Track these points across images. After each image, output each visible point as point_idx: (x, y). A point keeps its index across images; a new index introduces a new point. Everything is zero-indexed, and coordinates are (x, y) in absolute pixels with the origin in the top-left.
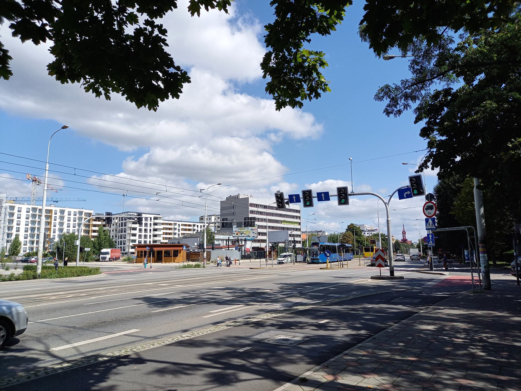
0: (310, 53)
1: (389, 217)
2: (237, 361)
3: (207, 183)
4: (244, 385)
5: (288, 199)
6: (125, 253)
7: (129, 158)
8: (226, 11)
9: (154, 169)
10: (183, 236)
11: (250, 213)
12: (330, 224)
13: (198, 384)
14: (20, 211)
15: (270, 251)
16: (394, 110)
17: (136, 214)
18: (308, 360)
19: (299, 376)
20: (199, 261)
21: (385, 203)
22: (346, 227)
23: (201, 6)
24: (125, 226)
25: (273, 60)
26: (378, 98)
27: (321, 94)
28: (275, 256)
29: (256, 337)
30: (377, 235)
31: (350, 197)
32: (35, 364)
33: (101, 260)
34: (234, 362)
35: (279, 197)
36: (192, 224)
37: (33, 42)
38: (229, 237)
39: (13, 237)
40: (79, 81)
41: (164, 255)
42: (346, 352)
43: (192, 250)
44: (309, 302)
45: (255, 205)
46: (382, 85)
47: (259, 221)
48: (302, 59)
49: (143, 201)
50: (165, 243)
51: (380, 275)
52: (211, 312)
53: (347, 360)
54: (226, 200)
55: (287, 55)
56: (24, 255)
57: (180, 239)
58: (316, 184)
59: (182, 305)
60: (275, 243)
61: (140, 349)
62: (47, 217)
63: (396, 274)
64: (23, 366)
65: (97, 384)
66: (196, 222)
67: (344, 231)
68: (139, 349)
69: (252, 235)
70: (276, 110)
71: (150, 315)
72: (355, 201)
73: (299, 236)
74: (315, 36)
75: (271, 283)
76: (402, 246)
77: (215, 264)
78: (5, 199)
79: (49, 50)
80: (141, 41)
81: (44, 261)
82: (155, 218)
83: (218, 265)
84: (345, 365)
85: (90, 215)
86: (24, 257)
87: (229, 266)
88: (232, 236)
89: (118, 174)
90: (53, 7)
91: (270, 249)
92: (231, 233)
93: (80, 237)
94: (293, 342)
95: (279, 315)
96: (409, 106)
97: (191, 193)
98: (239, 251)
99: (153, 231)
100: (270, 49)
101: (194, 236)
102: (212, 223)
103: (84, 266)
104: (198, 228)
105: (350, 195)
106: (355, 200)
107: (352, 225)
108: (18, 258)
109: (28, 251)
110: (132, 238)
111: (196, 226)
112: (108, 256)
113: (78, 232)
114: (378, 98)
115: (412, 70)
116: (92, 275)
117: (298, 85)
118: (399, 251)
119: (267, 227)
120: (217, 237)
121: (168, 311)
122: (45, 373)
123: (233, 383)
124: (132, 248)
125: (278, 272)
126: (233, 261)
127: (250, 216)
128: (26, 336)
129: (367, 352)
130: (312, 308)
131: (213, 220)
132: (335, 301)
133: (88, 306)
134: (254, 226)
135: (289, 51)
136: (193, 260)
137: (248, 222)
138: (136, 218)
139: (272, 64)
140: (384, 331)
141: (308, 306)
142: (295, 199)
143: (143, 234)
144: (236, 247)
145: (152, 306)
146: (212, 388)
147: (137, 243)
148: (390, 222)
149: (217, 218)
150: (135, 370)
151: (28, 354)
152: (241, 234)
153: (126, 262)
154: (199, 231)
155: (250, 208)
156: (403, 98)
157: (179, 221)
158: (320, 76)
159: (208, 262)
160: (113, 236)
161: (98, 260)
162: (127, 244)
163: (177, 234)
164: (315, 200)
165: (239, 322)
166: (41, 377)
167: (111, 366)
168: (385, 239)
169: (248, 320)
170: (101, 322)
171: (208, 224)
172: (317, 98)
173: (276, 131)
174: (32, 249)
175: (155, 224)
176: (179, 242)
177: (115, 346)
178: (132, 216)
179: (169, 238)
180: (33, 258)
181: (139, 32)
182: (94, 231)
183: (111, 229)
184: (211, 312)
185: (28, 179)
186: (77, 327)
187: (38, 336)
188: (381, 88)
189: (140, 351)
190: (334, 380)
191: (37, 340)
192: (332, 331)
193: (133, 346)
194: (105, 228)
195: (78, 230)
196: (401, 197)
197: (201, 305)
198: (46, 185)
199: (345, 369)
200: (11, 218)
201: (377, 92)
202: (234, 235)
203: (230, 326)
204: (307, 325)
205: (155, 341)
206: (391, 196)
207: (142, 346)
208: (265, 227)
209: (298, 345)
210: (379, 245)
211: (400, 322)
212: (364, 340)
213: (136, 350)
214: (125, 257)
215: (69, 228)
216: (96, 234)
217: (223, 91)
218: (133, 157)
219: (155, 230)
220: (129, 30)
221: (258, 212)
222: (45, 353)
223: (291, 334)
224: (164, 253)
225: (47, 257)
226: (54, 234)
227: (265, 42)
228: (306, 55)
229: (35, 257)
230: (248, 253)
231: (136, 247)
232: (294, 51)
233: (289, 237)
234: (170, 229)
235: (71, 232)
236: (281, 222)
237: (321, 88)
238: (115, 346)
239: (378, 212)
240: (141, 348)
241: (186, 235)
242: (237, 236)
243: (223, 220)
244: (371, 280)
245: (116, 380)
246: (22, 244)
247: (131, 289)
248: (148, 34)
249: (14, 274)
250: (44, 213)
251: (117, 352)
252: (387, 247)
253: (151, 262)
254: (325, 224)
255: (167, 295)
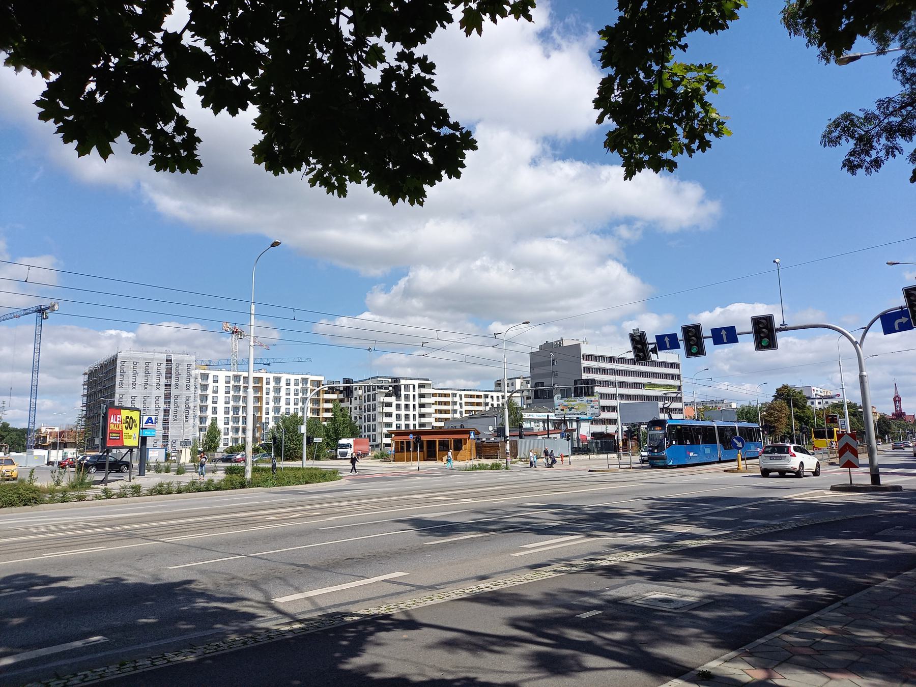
0: (688, 69)
1: (864, 370)
2: (575, 634)
3: (505, 321)
4: (593, 678)
5: (655, 343)
6: (376, 445)
7: (376, 287)
8: (529, 18)
9: (416, 303)
10: (468, 415)
11: (584, 372)
12: (741, 387)
13: (512, 670)
14: (217, 382)
15: (625, 439)
16: (864, 161)
17: (390, 380)
18: (711, 640)
19: (697, 667)
20: (497, 458)
21: (855, 343)
22: (774, 393)
23: (483, 16)
24: (374, 400)
25: (618, 91)
26: (830, 140)
27: (711, 142)
28: (635, 449)
29: (608, 593)
30: (841, 406)
31: (778, 334)
32: (252, 623)
33: (340, 457)
34: (572, 635)
35: (638, 341)
36: (482, 393)
37: (228, 112)
38: (548, 415)
39: (209, 422)
40: (299, 169)
41: (439, 449)
42: (788, 628)
43: (484, 439)
44: (706, 533)
45: (593, 357)
46: (836, 115)
47: (602, 385)
48: (673, 82)
49: (401, 358)
50: (440, 427)
51: (849, 483)
52: (524, 546)
53: (792, 644)
54: (539, 350)
55: (644, 78)
56: (225, 451)
57: (463, 419)
58: (710, 312)
59: (475, 532)
60: (634, 425)
61: (411, 605)
62: (258, 389)
63: (885, 481)
64: (234, 624)
65: (346, 659)
66: (489, 391)
67: (770, 399)
68: (408, 605)
69: (589, 411)
70: (625, 179)
71: (423, 550)
72: (791, 341)
73: (680, 411)
74: (696, 38)
75: (631, 497)
76: (893, 426)
77: (525, 463)
78: (194, 364)
79: (253, 124)
80: (393, 89)
81: (255, 460)
82: (421, 386)
83: (531, 465)
84: (787, 653)
85: (318, 383)
86: (225, 453)
87: (550, 467)
88: (554, 414)
89: (359, 314)
90: (256, 51)
91: (625, 435)
92: (552, 408)
93: (305, 420)
94: (680, 605)
95: (649, 555)
96: (897, 149)
97: (480, 341)
98: (568, 440)
99: (419, 407)
100: (611, 71)
101: (487, 415)
102: (518, 391)
103: (314, 467)
104: (493, 401)
105: (780, 330)
106: (790, 339)
107: (785, 387)
108: (218, 455)
109: (230, 444)
110: (386, 420)
111: (489, 397)
112: (350, 451)
113: (303, 413)
114: (830, 140)
115: (900, 78)
116: (328, 481)
117: (665, 129)
118: (888, 436)
119: (617, 396)
120: (526, 415)
121: (451, 543)
122: (266, 637)
123: (573, 673)
124: (387, 436)
125: (642, 478)
126: (557, 457)
127: (584, 378)
128: (236, 578)
129: (831, 629)
130: (714, 543)
131: (518, 387)
132: (759, 532)
133: (324, 532)
134: (592, 394)
135: (648, 73)
136: (488, 456)
137: (582, 388)
138: (390, 386)
139: (616, 97)
140: (865, 592)
141: (705, 540)
142: (666, 342)
143: (403, 412)
144: (561, 433)
145: (425, 534)
146: (539, 678)
147: (394, 428)
148: (866, 379)
149: (525, 383)
150: (406, 640)
151: (240, 607)
152: (570, 410)
153: (379, 460)
154: (495, 406)
155: (583, 362)
156: (884, 135)
157: (461, 390)
158: (708, 109)
159: (514, 460)
160: (355, 418)
161: (335, 458)
162: (379, 430)
163: (458, 412)
164: (708, 343)
165: (577, 566)
166: (262, 643)
167: (365, 631)
168: (858, 413)
169: (593, 562)
170: (345, 558)
171: (509, 394)
172: (704, 151)
173: (629, 221)
174: (236, 440)
175: (422, 396)
176: (462, 426)
177: (369, 599)
178: (385, 384)
179: (446, 419)
180: (238, 454)
181: (389, 75)
182: (327, 410)
183: (353, 406)
184: (524, 546)
185: (226, 330)
186: (309, 566)
187: (253, 578)
188: (834, 122)
189: (410, 609)
190: (768, 679)
191: (251, 585)
192: (756, 589)
193: (398, 600)
194: (343, 405)
195: (303, 409)
196: (888, 329)
197: (507, 534)
198: (252, 338)
199: (787, 660)
200: (204, 393)
201: (825, 131)
202: (556, 412)
203: (560, 572)
204: (706, 575)
205: (434, 592)
206: (867, 329)
207: (414, 601)
208: (613, 396)
209: (690, 612)
210: (846, 424)
211: (901, 574)
212: (825, 608)
213: (405, 607)
214: (377, 452)
215: (290, 405)
216: (329, 415)
217: (532, 160)
218: (383, 285)
219: (422, 406)
220: (373, 75)
221: (599, 369)
222: (265, 606)
223: (676, 590)
224: (439, 445)
225: (258, 453)
226: (267, 416)
227: (600, 61)
228: (678, 74)
229: (242, 453)
230: (584, 444)
231: (393, 435)
232: (655, 68)
233: (660, 414)
234: (446, 403)
235: (292, 412)
236: (644, 386)
237: (712, 131)
238: (369, 599)
239: (838, 360)
240: (412, 603)
241: (473, 413)
242: (562, 413)
243: (536, 385)
244: (830, 492)
245: (375, 655)
246: (222, 433)
247: (389, 505)
248: (403, 75)
249: (212, 481)
250: (251, 384)
251: (374, 608)
252: (862, 428)
253: (418, 460)
254: (730, 388)
255: (448, 515)
